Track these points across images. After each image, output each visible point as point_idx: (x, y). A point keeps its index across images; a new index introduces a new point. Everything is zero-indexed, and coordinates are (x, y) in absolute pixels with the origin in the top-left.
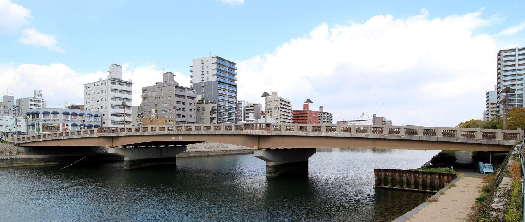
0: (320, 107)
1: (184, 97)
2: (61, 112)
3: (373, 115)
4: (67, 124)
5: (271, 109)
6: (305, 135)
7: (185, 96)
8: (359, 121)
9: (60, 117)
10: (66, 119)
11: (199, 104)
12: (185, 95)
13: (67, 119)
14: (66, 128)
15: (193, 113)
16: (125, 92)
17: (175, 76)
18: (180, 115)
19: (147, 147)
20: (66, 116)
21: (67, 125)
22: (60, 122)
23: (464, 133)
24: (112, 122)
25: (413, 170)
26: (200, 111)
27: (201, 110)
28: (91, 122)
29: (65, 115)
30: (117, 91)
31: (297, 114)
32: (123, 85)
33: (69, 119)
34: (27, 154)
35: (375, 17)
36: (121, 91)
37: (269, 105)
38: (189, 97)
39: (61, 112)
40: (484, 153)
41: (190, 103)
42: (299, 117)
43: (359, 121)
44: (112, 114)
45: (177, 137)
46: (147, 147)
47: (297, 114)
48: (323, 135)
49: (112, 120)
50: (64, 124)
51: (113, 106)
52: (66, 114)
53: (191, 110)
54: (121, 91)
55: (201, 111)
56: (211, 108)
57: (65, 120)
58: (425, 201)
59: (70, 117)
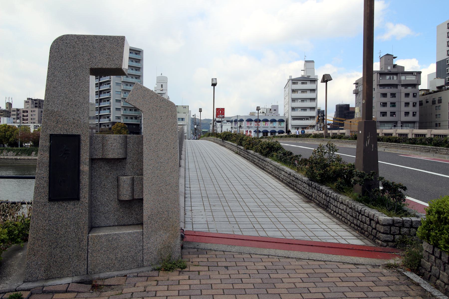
1: (395, 86)
2: (245, 120)
4: (250, 131)
7: (397, 85)
9: (244, 124)
10: (250, 126)
13: (251, 126)
14: (249, 135)
15: (410, 109)
16: (309, 91)
17: (395, 58)
18: (386, 112)
20: (250, 123)
21: (250, 132)
22: (244, 129)
24: (293, 126)
25: (205, 122)
26: (435, 104)
27: (437, 102)
28: (274, 127)
29: (248, 123)
30: (298, 91)
32: (306, 83)
33: (252, 125)
35: (171, 100)
36: (304, 91)
38: (406, 86)
39: (245, 120)
40: (335, 121)
44: (293, 117)
49: (293, 124)
50: (247, 131)
51: (294, 109)
52: (249, 120)
53: (407, 104)
54: (304, 91)
55: (437, 104)
57: (248, 127)
59: (253, 124)
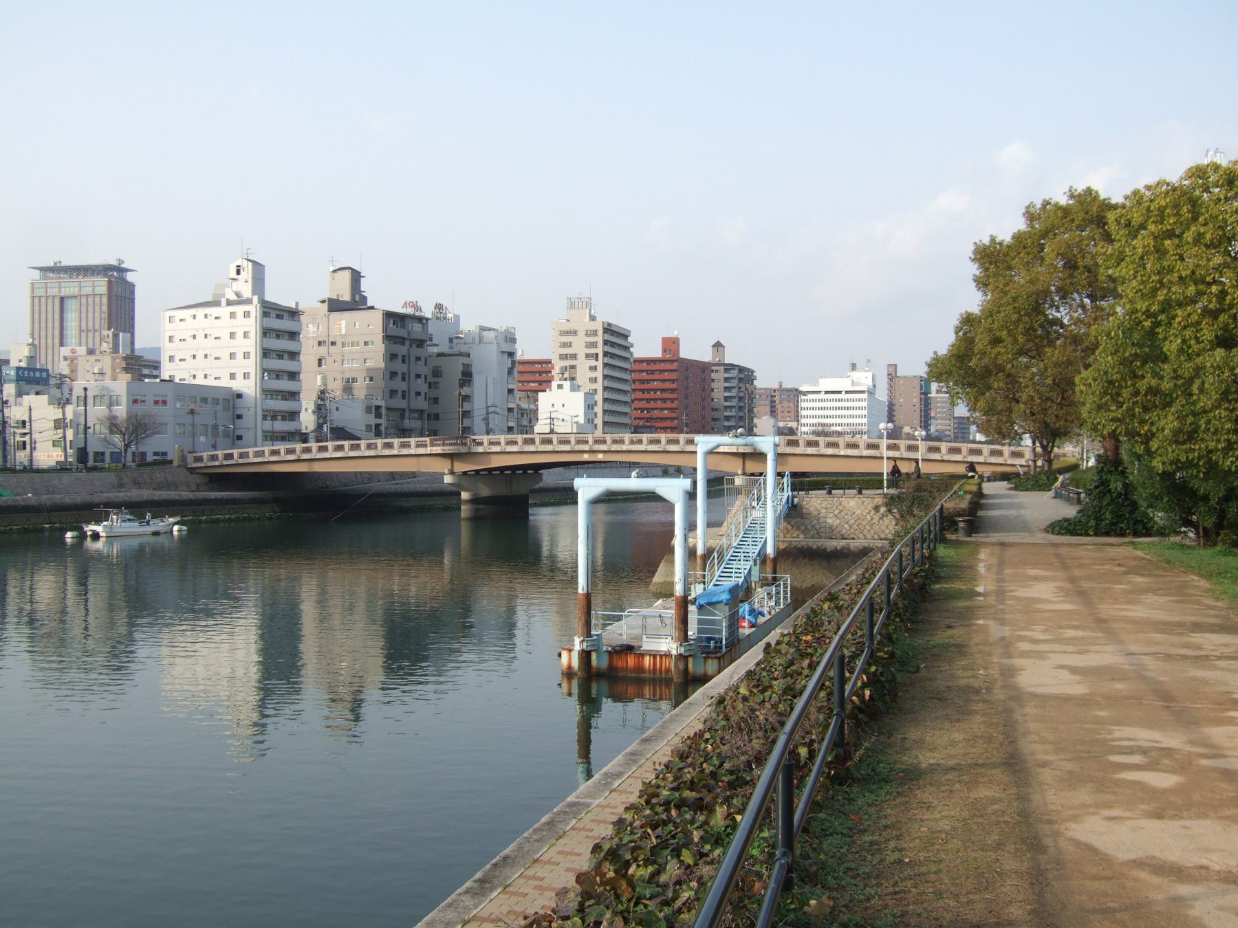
0: (714, 346)
3: (888, 370)
5: (574, 357)
6: (817, 453)
7: (404, 339)
8: (839, 392)
11: (440, 358)
12: (406, 336)
19: (525, 472)
23: (267, 576)
31: (643, 371)
34: (210, 490)
37: (569, 345)
41: (416, 357)
42: (648, 381)
43: (839, 392)
45: (592, 455)
46: (525, 472)
47: (643, 371)
48: (842, 453)
56: (461, 368)
58: (939, 370)
